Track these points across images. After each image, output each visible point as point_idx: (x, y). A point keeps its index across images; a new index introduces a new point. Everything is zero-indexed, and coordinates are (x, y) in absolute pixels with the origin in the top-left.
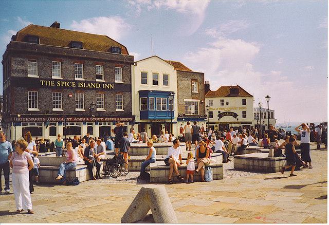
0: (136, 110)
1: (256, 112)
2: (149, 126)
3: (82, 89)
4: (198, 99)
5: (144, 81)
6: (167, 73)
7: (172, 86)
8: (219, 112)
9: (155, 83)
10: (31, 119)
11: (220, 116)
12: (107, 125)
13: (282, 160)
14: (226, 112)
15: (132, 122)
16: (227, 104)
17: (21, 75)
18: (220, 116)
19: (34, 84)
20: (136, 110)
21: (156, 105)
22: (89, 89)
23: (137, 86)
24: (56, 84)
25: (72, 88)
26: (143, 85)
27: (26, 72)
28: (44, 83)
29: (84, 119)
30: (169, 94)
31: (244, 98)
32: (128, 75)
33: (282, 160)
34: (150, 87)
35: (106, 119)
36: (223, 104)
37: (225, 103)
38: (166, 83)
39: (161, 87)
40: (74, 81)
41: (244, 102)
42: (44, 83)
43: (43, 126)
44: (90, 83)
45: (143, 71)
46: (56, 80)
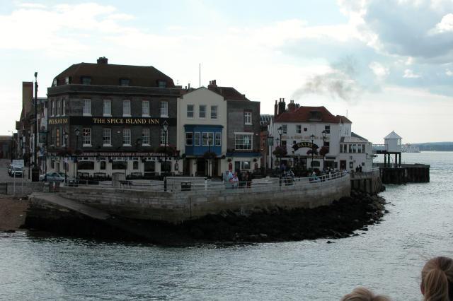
0: (181, 145)
1: (308, 181)
2: (194, 162)
3: (129, 126)
4: (250, 132)
5: (190, 115)
6: (192, 104)
7: (221, 120)
8: (295, 142)
9: (202, 115)
10: (85, 154)
11: (296, 147)
12: (152, 160)
13: (396, 160)
14: (304, 143)
15: (177, 158)
16: (306, 130)
17: (77, 115)
18: (296, 147)
19: (87, 122)
20: (181, 145)
21: (203, 143)
22: (135, 124)
23: (183, 119)
24: (106, 121)
25: (120, 124)
26: (201, 118)
27: (81, 111)
28: (97, 121)
29: (130, 154)
30: (220, 127)
31: (327, 125)
32: (173, 110)
33: (396, 160)
34: (197, 120)
35: (151, 154)
36: (300, 132)
37: (302, 129)
38: (214, 115)
39: (208, 121)
40: (122, 118)
41: (327, 130)
42: (97, 121)
43: (95, 160)
44: (137, 118)
45: (213, 105)
46: (106, 118)
